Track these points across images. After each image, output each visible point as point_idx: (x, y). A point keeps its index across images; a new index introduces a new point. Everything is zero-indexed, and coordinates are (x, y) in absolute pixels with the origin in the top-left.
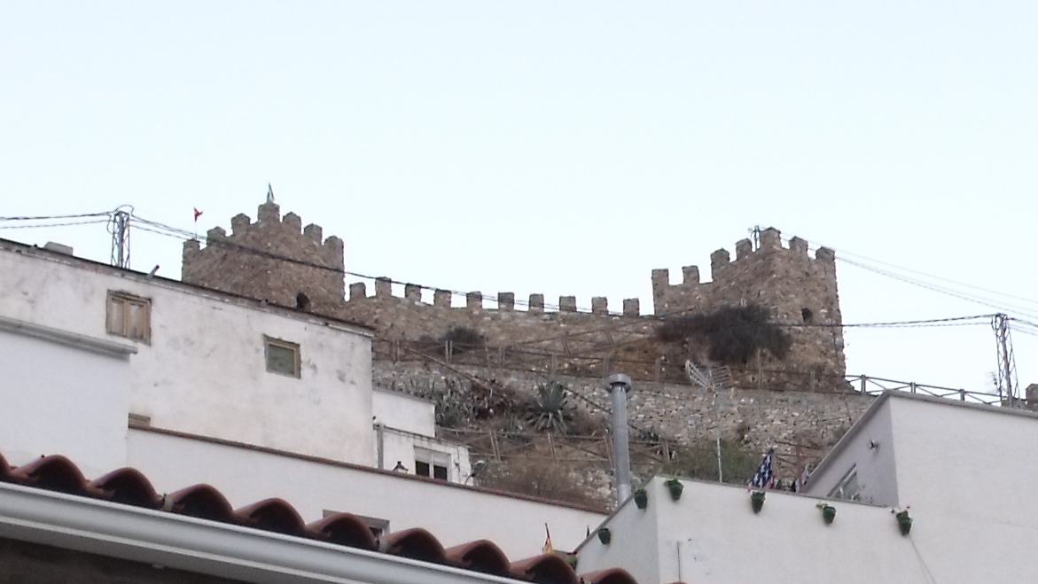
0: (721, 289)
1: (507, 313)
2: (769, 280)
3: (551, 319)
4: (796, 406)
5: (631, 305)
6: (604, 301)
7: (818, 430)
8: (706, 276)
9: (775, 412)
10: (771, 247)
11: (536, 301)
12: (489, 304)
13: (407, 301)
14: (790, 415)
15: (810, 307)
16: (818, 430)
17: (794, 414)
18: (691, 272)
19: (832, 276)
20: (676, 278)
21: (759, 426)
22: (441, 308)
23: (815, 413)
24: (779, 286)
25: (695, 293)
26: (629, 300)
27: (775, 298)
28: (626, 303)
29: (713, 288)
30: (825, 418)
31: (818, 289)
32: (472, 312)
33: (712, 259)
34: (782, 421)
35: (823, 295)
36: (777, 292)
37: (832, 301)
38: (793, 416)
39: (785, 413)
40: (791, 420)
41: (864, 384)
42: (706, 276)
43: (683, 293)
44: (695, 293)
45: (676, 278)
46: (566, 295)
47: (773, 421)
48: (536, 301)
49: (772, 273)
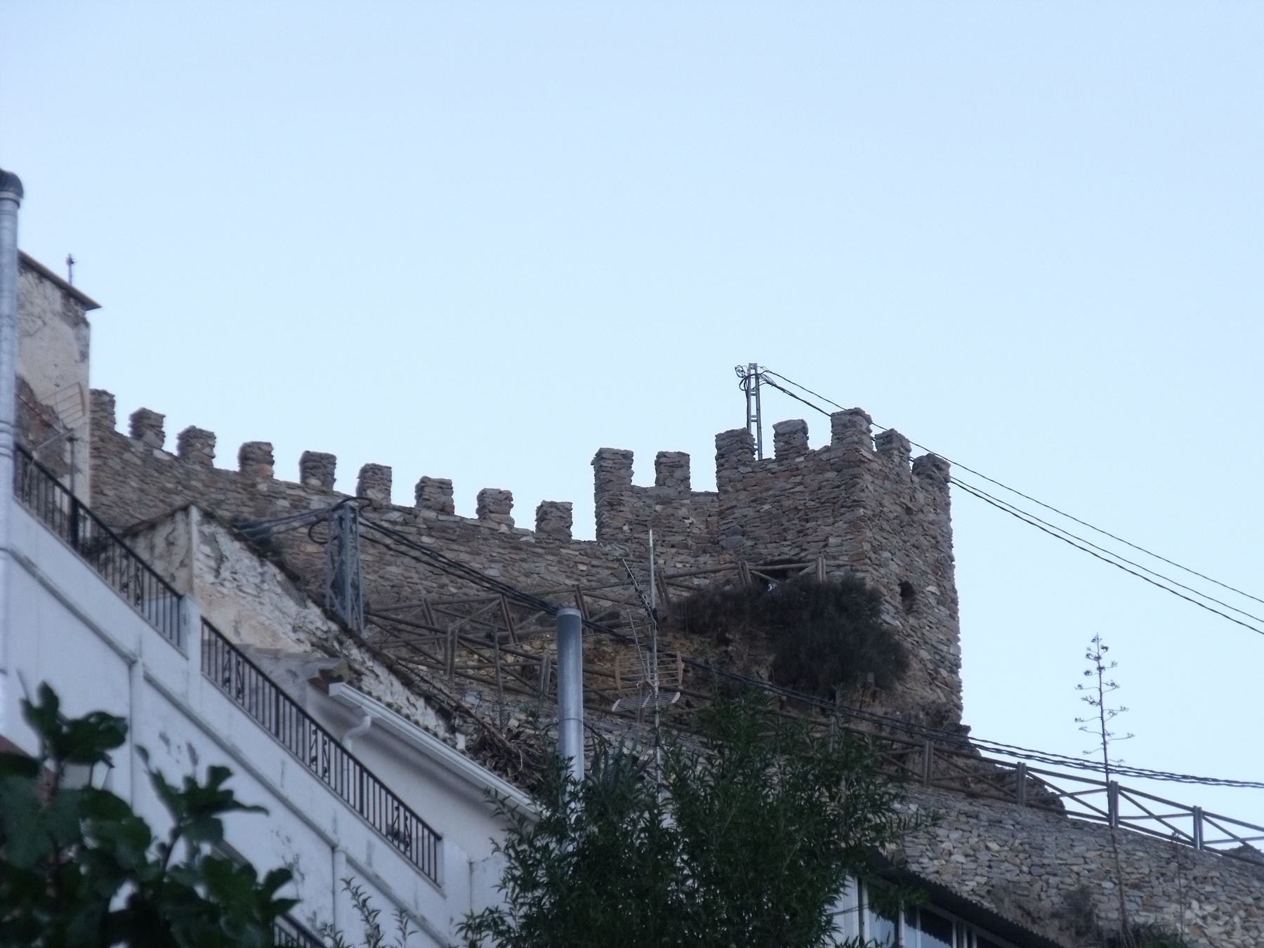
0: (738, 513)
1: (322, 497)
2: (848, 516)
3: (405, 523)
4: (993, 830)
5: (554, 516)
6: (445, 487)
7: (1030, 884)
8: (704, 478)
9: (955, 835)
10: (857, 450)
11: (375, 476)
12: (287, 470)
13: (139, 447)
14: (982, 846)
15: (913, 579)
16: (1030, 884)
17: (990, 844)
18: (673, 466)
19: (945, 517)
20: (644, 476)
21: (925, 860)
22: (198, 467)
23: (1027, 847)
24: (869, 534)
25: (683, 512)
26: (553, 504)
27: (861, 557)
28: (424, 487)
29: (715, 507)
30: (1046, 861)
31: (925, 542)
32: (254, 485)
33: (718, 447)
34: (967, 856)
35: (931, 556)
36: (867, 546)
37: (943, 567)
38: (987, 848)
39: (974, 840)
40: (984, 857)
41: (1113, 804)
42: (704, 478)
43: (658, 508)
44: (683, 512)
45: (644, 476)
46: (435, 475)
47: (950, 854)
48: (375, 476)
49: (858, 503)
